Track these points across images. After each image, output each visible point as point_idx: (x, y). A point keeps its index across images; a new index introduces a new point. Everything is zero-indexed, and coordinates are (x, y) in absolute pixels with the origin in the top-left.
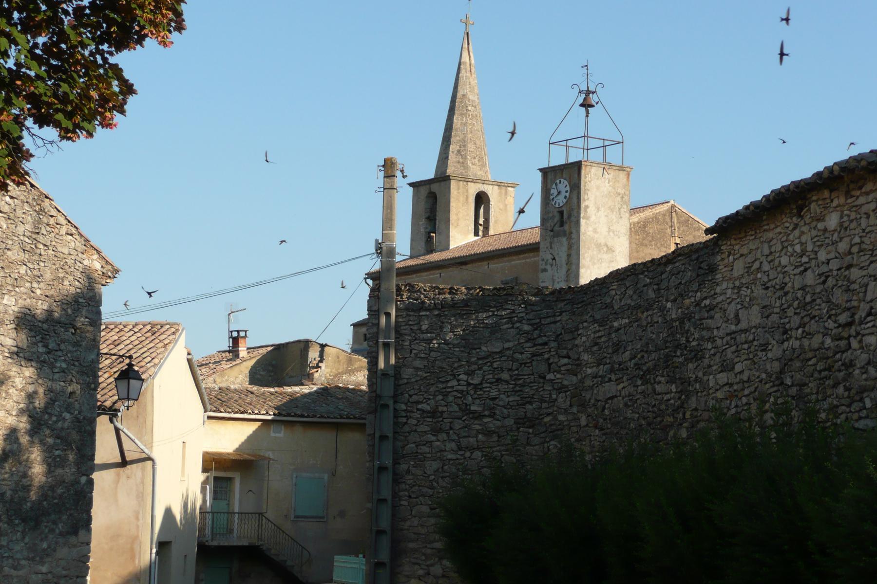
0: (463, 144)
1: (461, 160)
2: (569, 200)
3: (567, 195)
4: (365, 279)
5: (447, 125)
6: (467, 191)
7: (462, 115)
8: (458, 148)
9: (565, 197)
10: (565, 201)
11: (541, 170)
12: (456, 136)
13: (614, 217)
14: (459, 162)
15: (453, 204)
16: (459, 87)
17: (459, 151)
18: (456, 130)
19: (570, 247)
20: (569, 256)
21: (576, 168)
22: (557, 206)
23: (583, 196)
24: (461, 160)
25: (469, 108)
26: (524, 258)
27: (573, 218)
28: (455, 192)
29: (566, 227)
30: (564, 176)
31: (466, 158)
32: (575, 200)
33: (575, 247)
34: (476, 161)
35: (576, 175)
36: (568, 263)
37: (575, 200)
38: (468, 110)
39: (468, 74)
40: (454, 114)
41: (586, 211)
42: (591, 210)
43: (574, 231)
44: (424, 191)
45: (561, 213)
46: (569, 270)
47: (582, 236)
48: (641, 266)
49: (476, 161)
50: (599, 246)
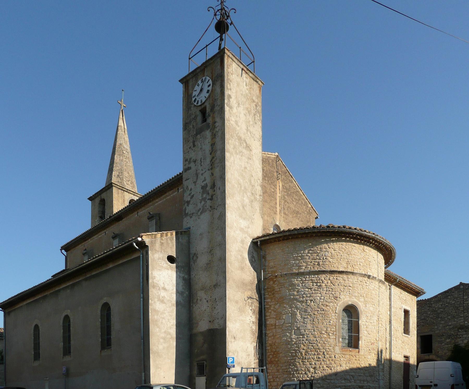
0: (121, 172)
1: (120, 181)
2: (211, 93)
3: (210, 88)
4: (61, 250)
5: (110, 166)
6: (124, 197)
7: (119, 155)
8: (118, 173)
9: (208, 91)
10: (207, 95)
11: (181, 81)
12: (116, 167)
13: (251, 118)
14: (118, 182)
15: (114, 202)
16: (118, 140)
17: (118, 176)
18: (116, 163)
19: (214, 136)
20: (213, 145)
21: (219, 60)
22: (199, 104)
23: (226, 85)
24: (120, 181)
25: (124, 152)
26: (165, 197)
27: (217, 108)
28: (116, 195)
29: (210, 120)
30: (206, 74)
31: (123, 180)
32: (218, 89)
33: (220, 133)
34: (129, 183)
35: (219, 67)
36: (213, 151)
37: (218, 89)
38: (123, 153)
39: (123, 133)
40: (115, 154)
41: (229, 100)
42: (233, 101)
43: (217, 119)
44: (97, 200)
45: (203, 112)
46: (213, 158)
47: (226, 122)
48: (219, 238)
49: (129, 183)
50: (240, 138)
